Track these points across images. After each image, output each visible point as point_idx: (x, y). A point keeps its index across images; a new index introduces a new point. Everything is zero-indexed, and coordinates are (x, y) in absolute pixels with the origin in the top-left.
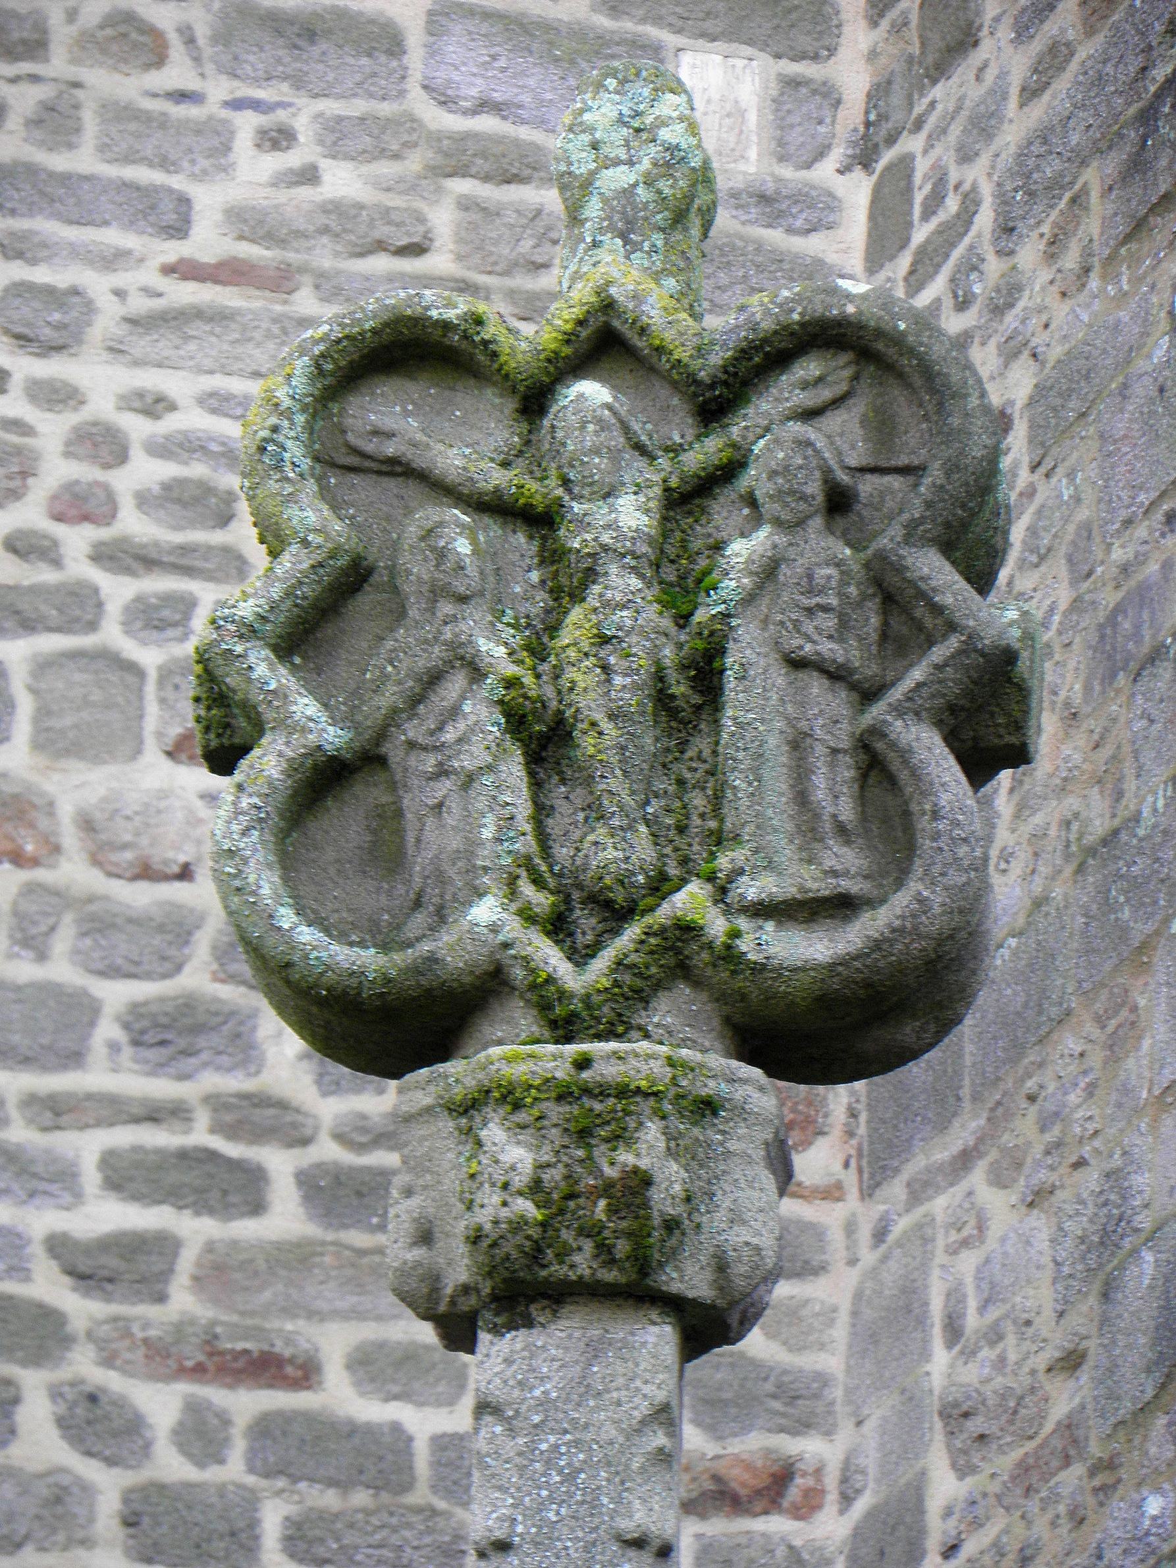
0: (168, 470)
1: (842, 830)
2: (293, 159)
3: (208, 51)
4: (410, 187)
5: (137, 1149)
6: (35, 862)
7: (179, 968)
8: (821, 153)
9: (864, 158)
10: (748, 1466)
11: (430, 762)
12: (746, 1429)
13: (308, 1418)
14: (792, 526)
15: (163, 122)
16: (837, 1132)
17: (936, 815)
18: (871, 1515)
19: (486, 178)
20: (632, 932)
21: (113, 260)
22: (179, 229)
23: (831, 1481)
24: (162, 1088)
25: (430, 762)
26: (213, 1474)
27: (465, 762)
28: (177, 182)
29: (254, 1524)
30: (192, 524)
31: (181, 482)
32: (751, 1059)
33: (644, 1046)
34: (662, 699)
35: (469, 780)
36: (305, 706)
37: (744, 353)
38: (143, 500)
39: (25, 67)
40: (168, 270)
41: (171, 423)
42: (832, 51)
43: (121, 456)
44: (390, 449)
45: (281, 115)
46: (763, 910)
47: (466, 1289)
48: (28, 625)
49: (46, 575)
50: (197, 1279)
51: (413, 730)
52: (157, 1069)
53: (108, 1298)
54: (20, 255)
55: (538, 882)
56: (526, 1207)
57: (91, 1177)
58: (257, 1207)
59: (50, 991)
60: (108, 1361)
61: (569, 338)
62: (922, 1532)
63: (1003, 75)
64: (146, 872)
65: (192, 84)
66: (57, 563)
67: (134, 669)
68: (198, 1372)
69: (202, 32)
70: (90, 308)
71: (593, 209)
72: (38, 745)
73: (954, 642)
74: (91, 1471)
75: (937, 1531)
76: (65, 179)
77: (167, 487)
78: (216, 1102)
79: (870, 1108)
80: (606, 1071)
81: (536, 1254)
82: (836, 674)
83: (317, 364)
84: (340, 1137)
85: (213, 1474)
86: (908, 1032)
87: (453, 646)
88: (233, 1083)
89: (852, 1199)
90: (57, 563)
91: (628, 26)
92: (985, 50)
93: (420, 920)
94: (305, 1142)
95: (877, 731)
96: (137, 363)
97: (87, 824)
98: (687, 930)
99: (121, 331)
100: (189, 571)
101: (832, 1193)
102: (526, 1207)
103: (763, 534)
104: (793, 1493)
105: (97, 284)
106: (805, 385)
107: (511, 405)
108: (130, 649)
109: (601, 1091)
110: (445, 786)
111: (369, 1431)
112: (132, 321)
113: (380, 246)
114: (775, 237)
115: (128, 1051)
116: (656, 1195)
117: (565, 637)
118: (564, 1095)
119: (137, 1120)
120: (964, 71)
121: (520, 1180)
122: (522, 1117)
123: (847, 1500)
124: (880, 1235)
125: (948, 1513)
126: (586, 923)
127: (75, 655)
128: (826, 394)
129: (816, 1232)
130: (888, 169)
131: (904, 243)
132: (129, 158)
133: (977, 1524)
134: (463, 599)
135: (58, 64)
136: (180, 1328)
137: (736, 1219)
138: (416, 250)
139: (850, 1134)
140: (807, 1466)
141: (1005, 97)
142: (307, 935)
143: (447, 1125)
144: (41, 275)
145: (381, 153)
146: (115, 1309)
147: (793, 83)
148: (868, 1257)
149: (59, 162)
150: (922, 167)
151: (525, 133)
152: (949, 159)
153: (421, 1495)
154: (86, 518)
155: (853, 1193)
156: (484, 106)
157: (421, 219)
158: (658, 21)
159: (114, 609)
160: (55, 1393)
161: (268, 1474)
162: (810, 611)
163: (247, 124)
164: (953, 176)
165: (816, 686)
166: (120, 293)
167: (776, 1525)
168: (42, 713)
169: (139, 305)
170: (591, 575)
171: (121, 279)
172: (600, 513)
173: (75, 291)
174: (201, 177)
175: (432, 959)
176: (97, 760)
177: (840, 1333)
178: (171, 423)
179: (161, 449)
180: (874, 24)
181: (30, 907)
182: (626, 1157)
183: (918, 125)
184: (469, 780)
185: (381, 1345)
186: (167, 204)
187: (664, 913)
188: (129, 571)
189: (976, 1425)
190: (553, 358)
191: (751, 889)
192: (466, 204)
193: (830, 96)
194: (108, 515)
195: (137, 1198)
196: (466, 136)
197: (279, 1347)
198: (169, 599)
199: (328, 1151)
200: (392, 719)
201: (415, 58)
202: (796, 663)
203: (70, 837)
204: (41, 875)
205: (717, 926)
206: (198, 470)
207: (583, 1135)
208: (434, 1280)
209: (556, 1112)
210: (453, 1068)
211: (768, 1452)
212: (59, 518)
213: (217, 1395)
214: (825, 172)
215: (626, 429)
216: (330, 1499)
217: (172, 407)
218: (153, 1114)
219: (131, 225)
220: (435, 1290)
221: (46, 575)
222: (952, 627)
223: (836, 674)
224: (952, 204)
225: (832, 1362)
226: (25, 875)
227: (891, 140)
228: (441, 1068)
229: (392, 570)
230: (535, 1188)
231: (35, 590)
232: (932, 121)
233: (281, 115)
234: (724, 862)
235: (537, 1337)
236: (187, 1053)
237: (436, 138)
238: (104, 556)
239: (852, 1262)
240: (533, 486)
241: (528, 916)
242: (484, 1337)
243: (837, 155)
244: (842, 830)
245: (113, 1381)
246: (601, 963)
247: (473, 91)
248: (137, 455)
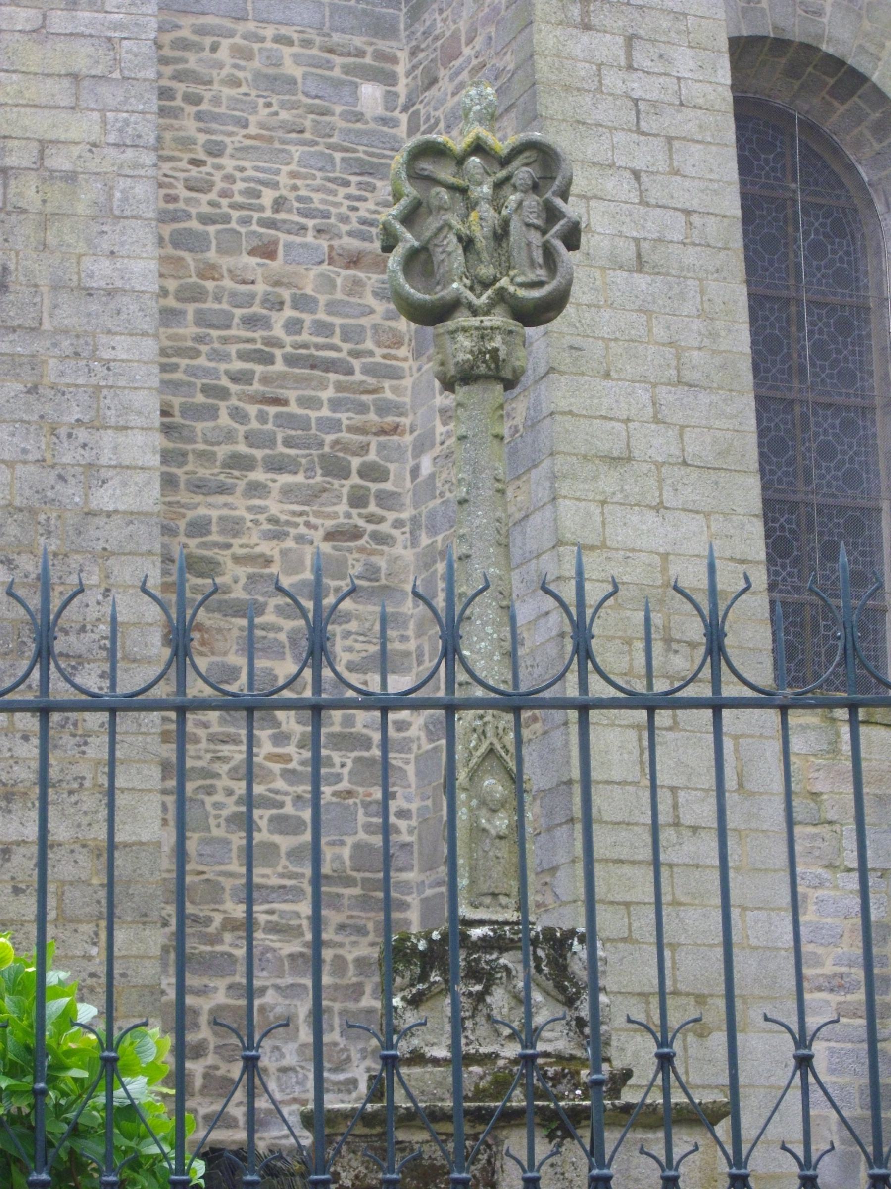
0: (246, 185)
2: (273, 109)
6: (218, 280)
8: (395, 108)
9: (405, 109)
11: (440, 249)
15: (241, 101)
21: (230, 134)
22: (246, 126)
23: (408, 428)
24: (249, 335)
26: (266, 427)
27: (449, 249)
28: (245, 115)
35: (450, 254)
36: (409, 236)
37: (512, 150)
38: (241, 193)
40: (244, 136)
43: (234, 182)
46: (522, 285)
49: (218, 211)
51: (436, 241)
52: (248, 330)
56: (469, 356)
58: (273, 363)
59: (223, 311)
60: (239, 400)
61: (469, 146)
62: (434, 439)
64: (244, 282)
66: (220, 207)
67: (239, 233)
71: (471, 115)
73: (566, 220)
74: (236, 425)
75: (438, 439)
78: (263, 338)
79: (416, 339)
80: (487, 323)
81: (472, 368)
85: (266, 427)
86: (552, 314)
87: (445, 221)
88: (265, 334)
91: (349, 78)
95: (548, 242)
96: (238, 159)
97: (230, 271)
98: (502, 289)
100: (251, 209)
101: (405, 359)
102: (469, 356)
104: (399, 431)
105: (227, 140)
107: (454, 163)
108: (238, 228)
109: (485, 329)
111: (301, 416)
112: (235, 149)
114: (385, 129)
117: (471, 219)
118: (477, 329)
123: (412, 432)
124: (419, 369)
126: (478, 289)
127: (225, 230)
129: (403, 369)
132: (234, 109)
135: (216, 86)
142: (412, 291)
144: (214, 137)
145: (293, 108)
146: (240, 387)
147: (388, 92)
149: (217, 110)
150: (423, 112)
151: (326, 104)
152: (431, 110)
153: (314, 431)
154: (226, 196)
155: (411, 359)
158: (357, 77)
159: (234, 218)
160: (228, 408)
161: (279, 426)
163: (261, 101)
168: (218, 244)
169: (237, 145)
170: (477, 203)
174: (250, 114)
177: (409, 392)
179: (243, 180)
182: (493, 345)
183: (422, 102)
184: (450, 254)
187: (498, 285)
189: (449, 413)
190: (465, 150)
191: (519, 280)
192: (313, 121)
193: (396, 95)
194: (232, 196)
195: (244, 361)
199: (288, 349)
200: (431, 239)
202: (528, 225)
203: (225, 274)
204: (219, 283)
205: (512, 289)
206: (252, 185)
207: (482, 337)
208: (445, 374)
209: (475, 333)
210: (449, 323)
213: (265, 408)
214: (396, 113)
216: (292, 433)
218: (248, 341)
220: (445, 378)
221: (218, 211)
223: (537, 228)
224: (432, 121)
225: (407, 400)
226: (215, 283)
227: (413, 105)
229: (428, 202)
230: (471, 352)
231: (215, 214)
233: (269, 99)
234: (512, 273)
237: (306, 105)
238: (232, 206)
239: (412, 375)
241: (465, 286)
242: (457, 388)
243: (399, 109)
244: (540, 266)
245: (241, 404)
248: (238, 181)
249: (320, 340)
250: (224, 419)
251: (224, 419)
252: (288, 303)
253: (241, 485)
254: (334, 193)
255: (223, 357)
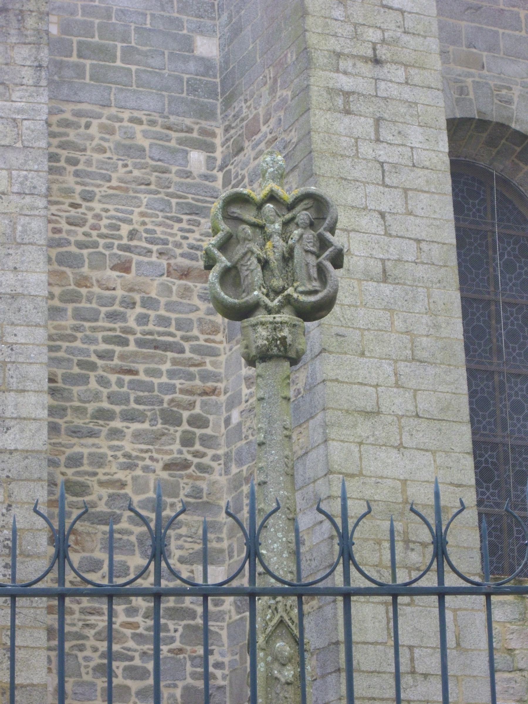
0: (109, 221)
1: (315, 279)
3: (113, 151)
4: (147, 174)
5: (108, 335)
6: (89, 287)
7: (113, 305)
8: (214, 168)
9: (221, 169)
10: (209, 388)
11: (245, 268)
12: (208, 382)
13: (138, 381)
14: (305, 228)
15: (106, 163)
16: (221, 332)
17: (331, 276)
18: (230, 396)
19: (160, 172)
20: (280, 297)
21: (99, 186)
22: (109, 181)
23: (222, 390)
24: (112, 325)
25: (245, 268)
26: (122, 390)
27: (252, 268)
29: (129, 398)
30: (114, 230)
31: (112, 223)
32: (299, 317)
33: (284, 315)
34: (283, 257)
35: (252, 271)
36: (223, 258)
37: (296, 199)
38: (105, 227)
39: (83, 153)
40: (108, 187)
41: (109, 214)
42: (215, 151)
44: (235, 215)
45: (126, 162)
46: (302, 293)
47: (254, 356)
48: (87, 247)
49: (90, 239)
50: (118, 357)
51: (242, 262)
52: (110, 322)
53: (104, 360)
54: (83, 185)
55: (264, 288)
56: (266, 342)
57: (100, 340)
58: (128, 345)
59: (93, 309)
60: (104, 371)
62: (241, 399)
63: (249, 155)
64: (108, 289)
65: (111, 156)
66: (91, 237)
67: (104, 255)
68: (119, 373)
69: (112, 147)
70: (95, 194)
71: (267, 175)
72: (89, 268)
73: (333, 247)
74: (102, 389)
75: (244, 398)
76: (91, 173)
77: (109, 224)
78: (121, 328)
80: (278, 319)
81: (268, 350)
82: (313, 253)
83: (224, 200)
84: (141, 333)
88: (123, 325)
89: (225, 344)
90: (91, 237)
92: (246, 151)
93: (244, 294)
94: (135, 334)
96: (104, 203)
97: (98, 281)
98: (289, 295)
99: (100, 198)
100: (113, 238)
102: (266, 342)
103: (300, 230)
104: (216, 392)
105: (96, 190)
106: (305, 204)
108: (104, 251)
110: (248, 272)
111: (147, 382)
113: (142, 184)
114: (207, 183)
115: (106, 319)
116: (287, 340)
117: (267, 247)
118: (271, 323)
119: (108, 330)
120: (241, 155)
121: (265, 338)
122: (264, 327)
123: (225, 393)
124: (231, 349)
125: (246, 395)
126: (272, 295)
127: (95, 252)
128: (309, 206)
129: (219, 349)
130: (227, 171)
131: (230, 183)
133: (252, 397)
134: (250, 240)
135: (88, 153)
136: (116, 365)
137: (300, 344)
138: (148, 184)
139: (224, 333)
140: (218, 387)
141: (250, 159)
142: (226, 297)
143: (250, 328)
144: (87, 188)
148: (228, 353)
149: (89, 169)
150: (233, 171)
154: (96, 229)
156: (159, 160)
157: (149, 179)
158: (187, 146)
159: (101, 245)
160: (96, 376)
162: (309, 242)
163: (120, 163)
164: (240, 172)
165: (310, 255)
166: (100, 191)
167: (214, 397)
171: (100, 189)
172: (272, 226)
173: (93, 191)
175: (247, 301)
176: (99, 270)
177: (223, 365)
178: (109, 214)
179: (108, 218)
180: (222, 147)
181: (88, 295)
182: (283, 334)
183: (232, 164)
185: (149, 368)
186: (107, 176)
187: (286, 293)
188: (103, 238)
189: (251, 380)
191: (301, 289)
193: (215, 159)
195: (108, 343)
196: (156, 165)
197: (132, 369)
198: (110, 243)
199: (139, 335)
200: (239, 260)
201: (147, 152)
203: (95, 283)
204: (90, 289)
205: (295, 295)
206: (114, 221)
208: (249, 354)
209: (270, 326)
210: (252, 319)
211: (212, 386)
212: (91, 229)
213: (122, 376)
214: (215, 172)
215: (276, 212)
216: (141, 394)
217: (109, 211)
218: (110, 330)
219: (101, 180)
220: (249, 357)
221: (90, 239)
222: (332, 245)
223: (313, 253)
224: (240, 177)
225: (222, 371)
227: (226, 166)
228: (249, 319)
229: (237, 236)
230: (267, 339)
231: (88, 241)
232: (235, 163)
234: (295, 284)
235: (267, 364)
236: (115, 319)
237: (151, 166)
238: (100, 236)
239: (225, 354)
240: (260, 221)
241: (263, 293)
242: (257, 364)
243: (217, 169)
244: (315, 279)
245: (105, 374)
246: (276, 301)
247: (157, 158)
249: (161, 329)
250: (93, 384)
251: (93, 384)
252: (138, 304)
253: (105, 431)
254: (172, 227)
255: (93, 341)
